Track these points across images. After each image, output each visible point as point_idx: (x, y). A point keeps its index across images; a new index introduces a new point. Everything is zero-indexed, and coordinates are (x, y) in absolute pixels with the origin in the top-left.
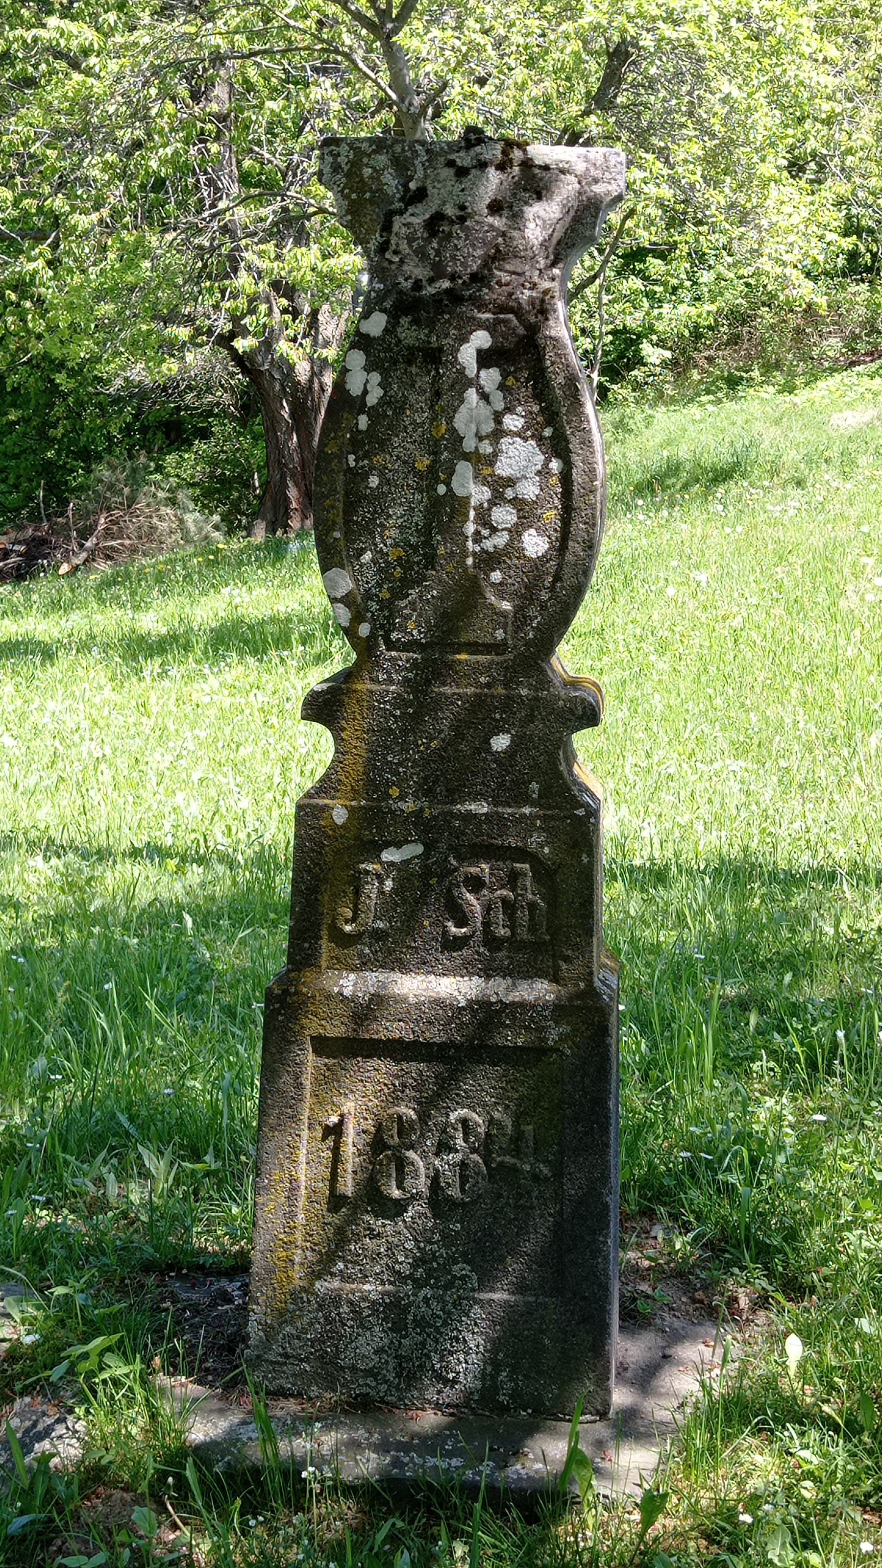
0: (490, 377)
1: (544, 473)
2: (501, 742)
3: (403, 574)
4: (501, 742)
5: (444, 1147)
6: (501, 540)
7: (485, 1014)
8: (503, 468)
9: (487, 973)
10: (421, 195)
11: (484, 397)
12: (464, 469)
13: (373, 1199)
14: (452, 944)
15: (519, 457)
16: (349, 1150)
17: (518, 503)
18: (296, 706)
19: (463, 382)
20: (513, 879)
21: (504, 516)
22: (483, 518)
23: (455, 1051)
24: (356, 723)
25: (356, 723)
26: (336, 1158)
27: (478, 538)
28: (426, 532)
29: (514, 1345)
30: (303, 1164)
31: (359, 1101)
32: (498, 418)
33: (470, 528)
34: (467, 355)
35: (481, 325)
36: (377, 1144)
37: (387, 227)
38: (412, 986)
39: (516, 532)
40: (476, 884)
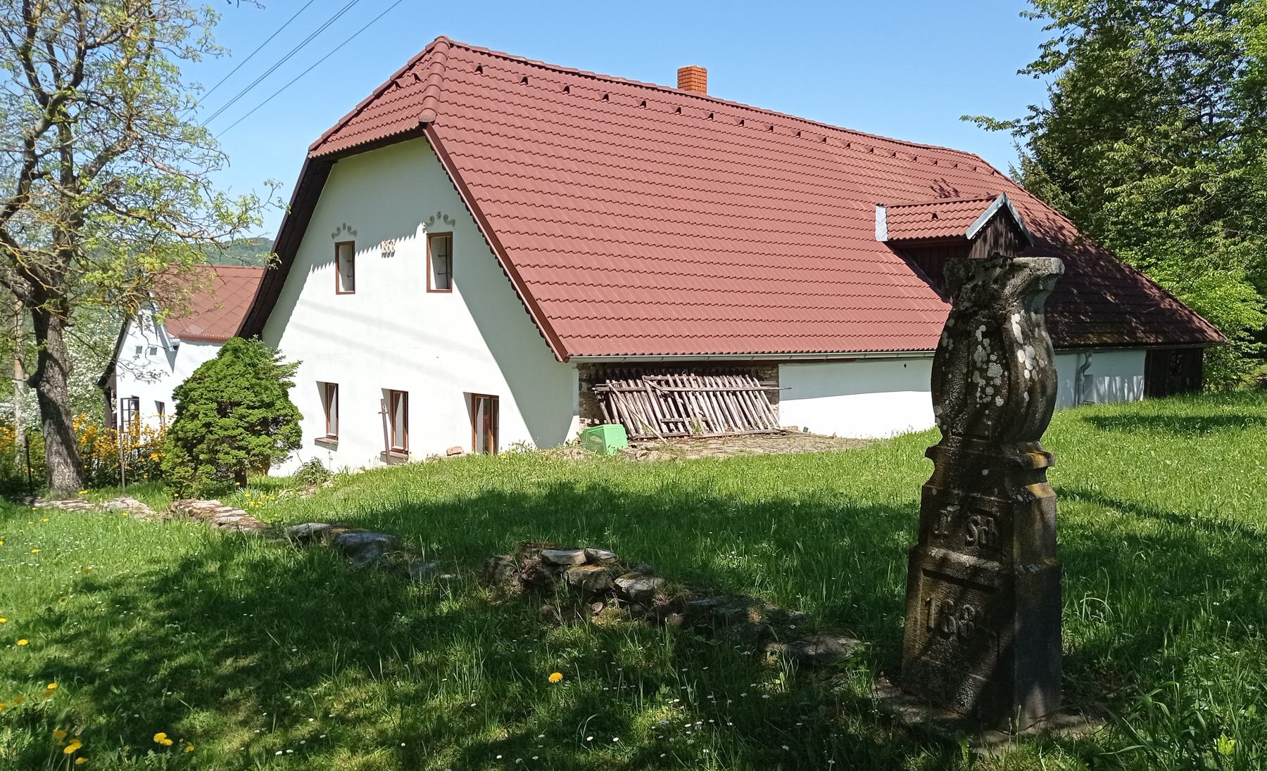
0: (986, 342)
1: (1003, 376)
2: (985, 472)
3: (962, 405)
4: (985, 472)
5: (962, 617)
6: (989, 399)
7: (975, 570)
8: (990, 374)
9: (980, 556)
10: (973, 278)
11: (984, 348)
12: (977, 373)
13: (938, 630)
14: (969, 544)
15: (995, 370)
16: (933, 611)
17: (994, 386)
18: (923, 452)
19: (977, 343)
20: (988, 523)
21: (990, 390)
22: (983, 391)
23: (968, 581)
24: (941, 460)
25: (941, 460)
26: (929, 614)
27: (981, 398)
28: (965, 395)
29: (984, 694)
30: (918, 612)
31: (939, 597)
32: (988, 355)
33: (978, 394)
34: (979, 334)
35: (983, 323)
36: (941, 611)
37: (960, 290)
38: (956, 556)
39: (993, 397)
40: (976, 523)
